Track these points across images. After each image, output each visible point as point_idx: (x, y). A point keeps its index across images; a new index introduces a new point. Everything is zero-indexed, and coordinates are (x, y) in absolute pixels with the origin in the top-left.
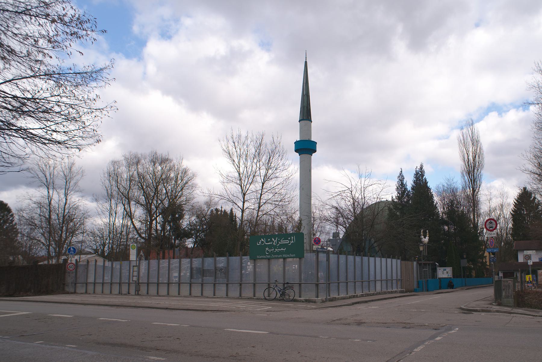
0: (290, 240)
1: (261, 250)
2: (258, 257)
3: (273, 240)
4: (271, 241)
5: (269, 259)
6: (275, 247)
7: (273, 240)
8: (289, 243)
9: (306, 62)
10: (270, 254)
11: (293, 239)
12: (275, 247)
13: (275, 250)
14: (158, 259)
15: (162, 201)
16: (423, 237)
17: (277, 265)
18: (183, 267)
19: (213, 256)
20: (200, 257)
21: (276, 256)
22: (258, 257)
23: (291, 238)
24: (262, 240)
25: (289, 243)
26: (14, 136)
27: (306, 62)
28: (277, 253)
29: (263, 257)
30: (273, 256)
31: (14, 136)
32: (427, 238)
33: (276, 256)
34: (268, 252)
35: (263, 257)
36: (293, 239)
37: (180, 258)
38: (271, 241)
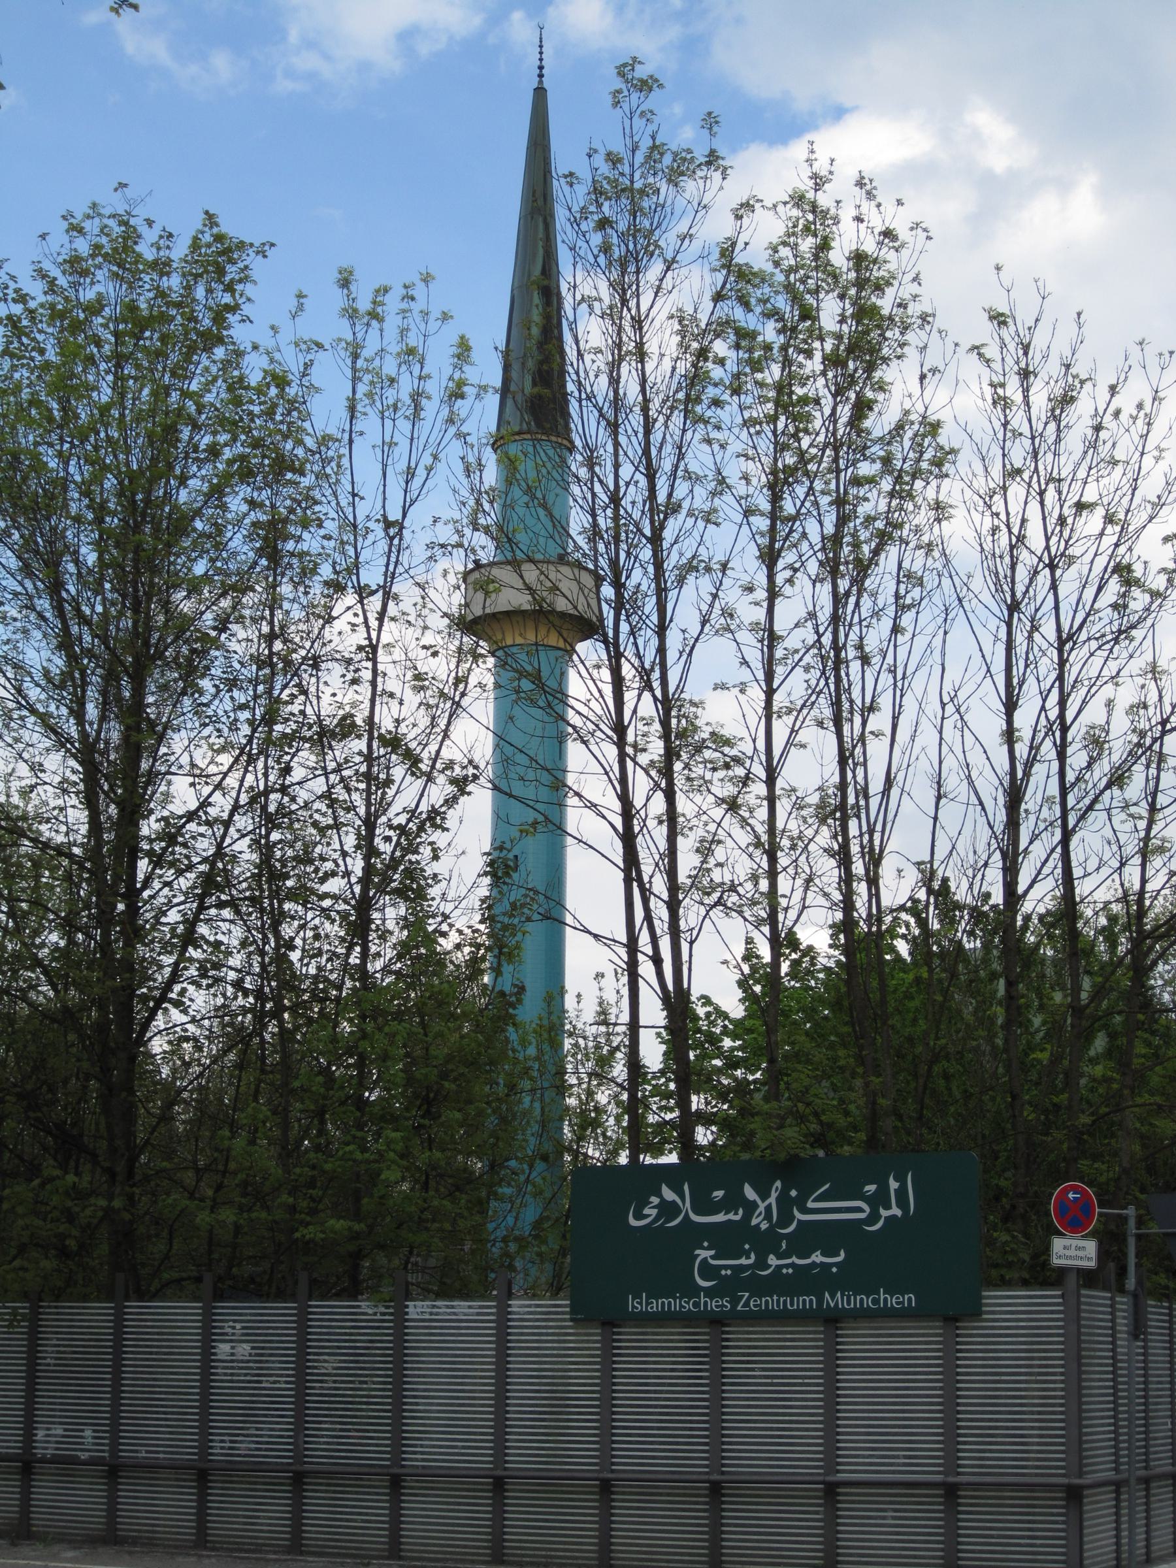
0: (879, 1200)
2: (635, 1305)
3: (750, 1193)
5: (717, 1321)
6: (766, 1243)
7: (750, 1193)
8: (873, 1218)
9: (540, 93)
10: (729, 1286)
12: (766, 1243)
13: (762, 1263)
15: (637, 525)
17: (775, 1371)
20: (280, 1296)
21: (773, 1302)
22: (635, 1305)
24: (668, 1194)
25: (873, 1218)
27: (540, 93)
29: (675, 1304)
30: (748, 1301)
33: (773, 1302)
34: (708, 1271)
35: (675, 1304)
38: (734, 1200)
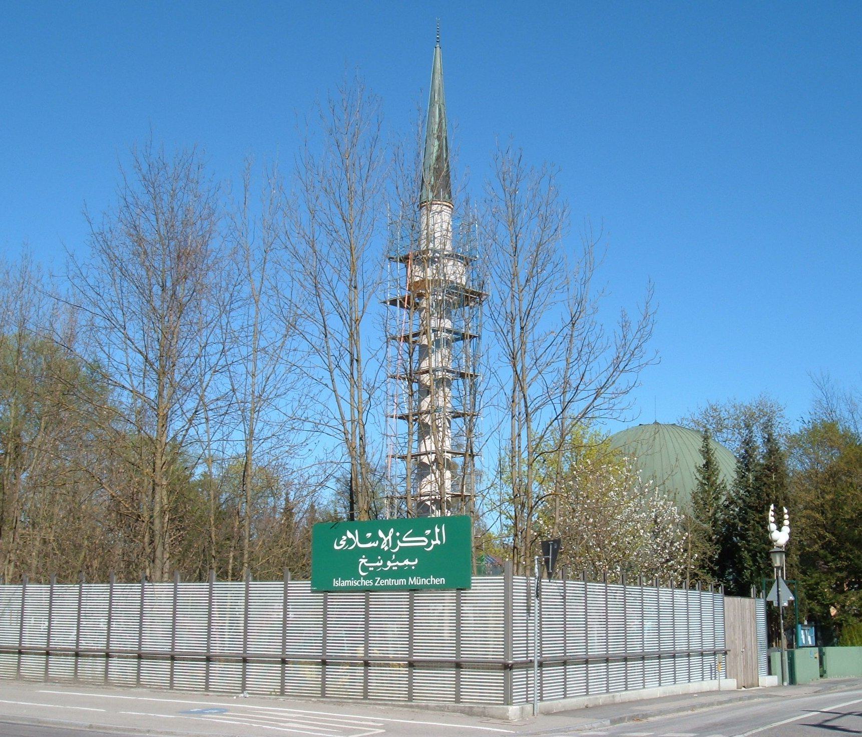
0: (431, 537)
1: (347, 563)
2: (337, 583)
3: (381, 534)
4: (375, 537)
5: (367, 590)
6: (387, 556)
7: (381, 534)
10: (372, 575)
11: (440, 534)
12: (387, 556)
13: (385, 565)
14: (175, 582)
16: (773, 527)
18: (646, 600)
19: (280, 578)
21: (389, 582)
22: (337, 583)
23: (433, 532)
24: (350, 535)
26: (427, 224)
28: (391, 574)
30: (381, 582)
31: (427, 224)
32: (786, 530)
34: (365, 568)
36: (440, 534)
37: (565, 578)
38: (375, 537)
